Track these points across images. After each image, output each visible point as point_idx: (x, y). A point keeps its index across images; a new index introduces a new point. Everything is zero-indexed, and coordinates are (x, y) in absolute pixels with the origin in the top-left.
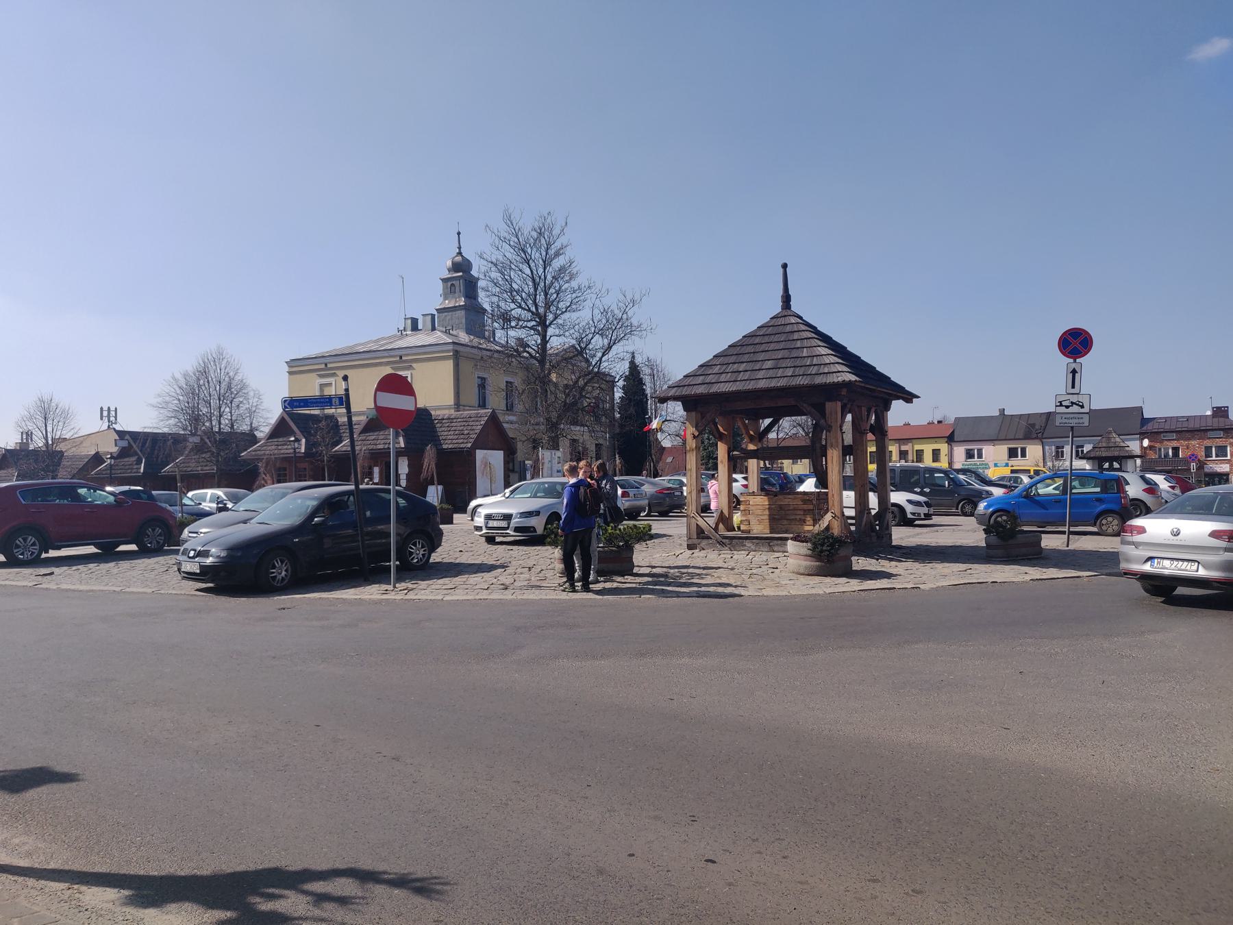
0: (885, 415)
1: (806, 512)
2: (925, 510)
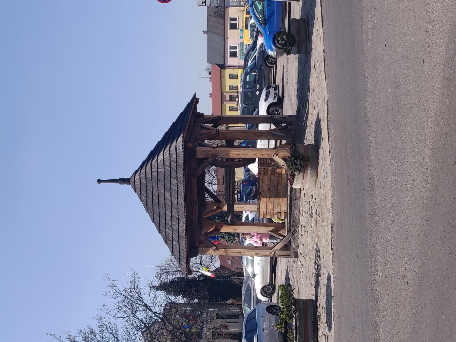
0: (206, 117)
1: (272, 173)
2: (272, 90)
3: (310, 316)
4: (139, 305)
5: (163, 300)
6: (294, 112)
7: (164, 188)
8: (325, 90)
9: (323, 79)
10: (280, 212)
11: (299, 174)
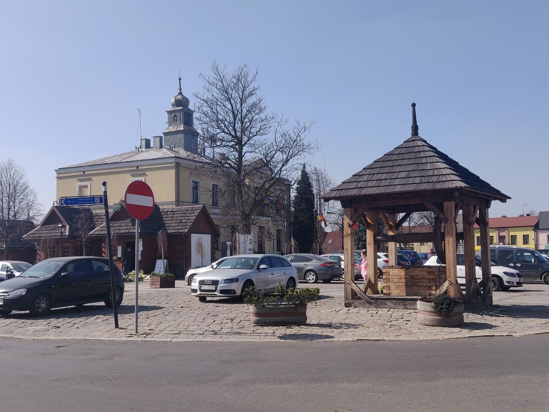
3: (291, 318)
4: (287, 154)
5: (293, 177)
6: (495, 302)
7: (410, 170)
8: (523, 333)
9: (536, 331)
10: (390, 289)
11: (432, 307)
